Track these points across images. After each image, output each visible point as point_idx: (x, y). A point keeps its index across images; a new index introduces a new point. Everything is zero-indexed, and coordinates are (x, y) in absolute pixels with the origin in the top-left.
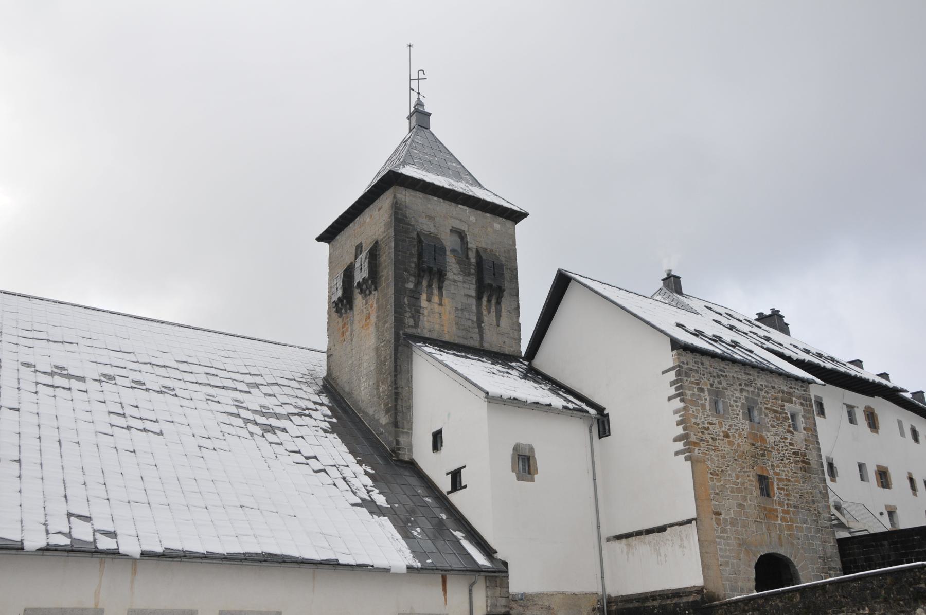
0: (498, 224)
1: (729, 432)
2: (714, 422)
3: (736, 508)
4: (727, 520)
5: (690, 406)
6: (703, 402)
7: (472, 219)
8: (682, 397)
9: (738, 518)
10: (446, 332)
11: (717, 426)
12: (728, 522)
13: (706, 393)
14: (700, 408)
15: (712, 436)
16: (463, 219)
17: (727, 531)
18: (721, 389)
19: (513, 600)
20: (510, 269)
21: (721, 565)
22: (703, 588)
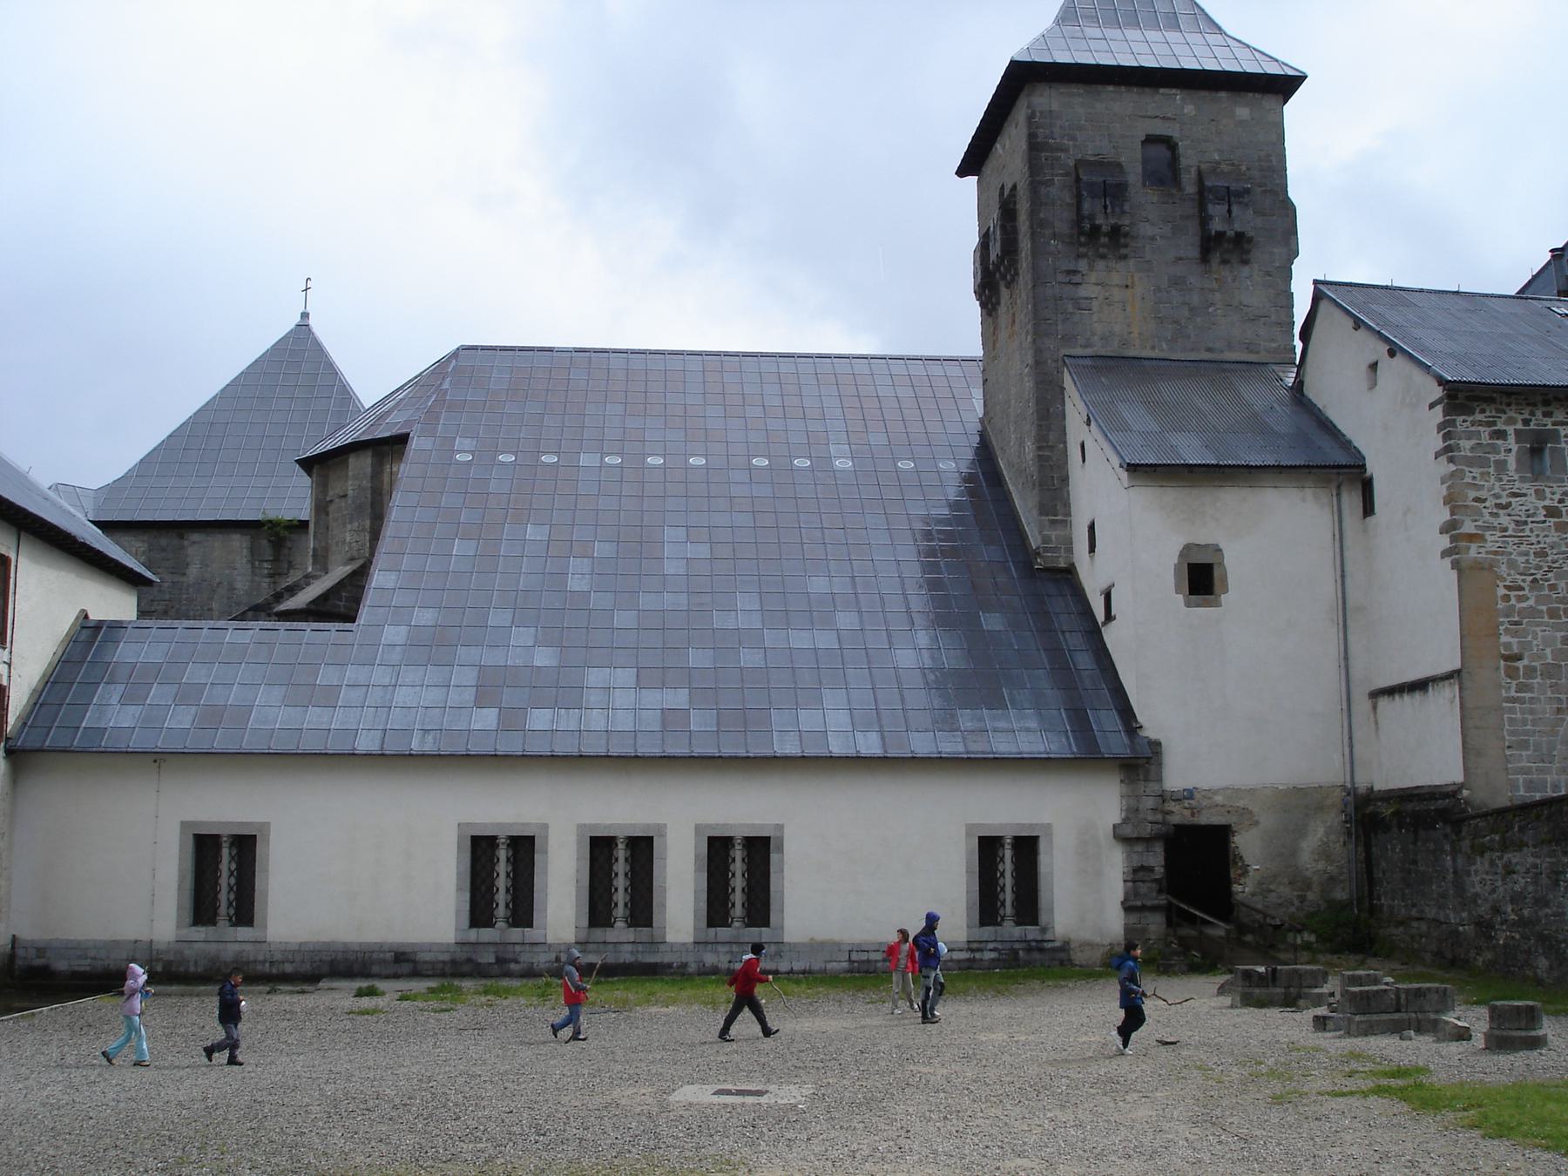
0: (1243, 110)
1: (1560, 505)
2: (1524, 491)
3: (1559, 644)
4: (1534, 669)
5: (1467, 469)
6: (1502, 456)
7: (1189, 109)
8: (1450, 454)
9: (1563, 663)
10: (1137, 335)
11: (1532, 498)
12: (1536, 671)
13: (1511, 439)
14: (1491, 470)
15: (1518, 518)
16: (1169, 115)
17: (1533, 688)
18: (1549, 427)
19: (1173, 800)
20: (1270, 191)
21: (1509, 747)
22: (1462, 786)
